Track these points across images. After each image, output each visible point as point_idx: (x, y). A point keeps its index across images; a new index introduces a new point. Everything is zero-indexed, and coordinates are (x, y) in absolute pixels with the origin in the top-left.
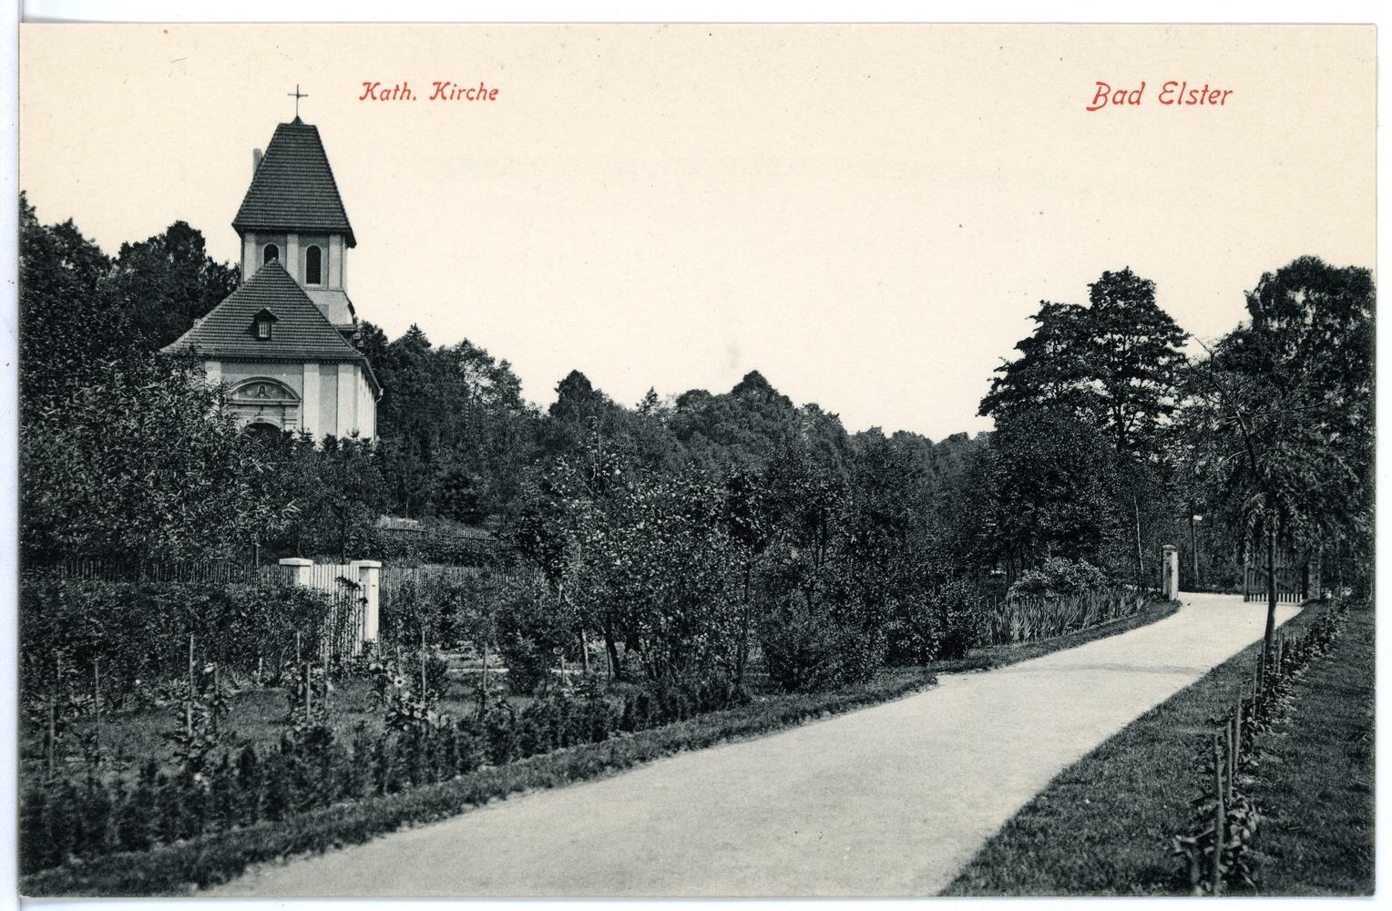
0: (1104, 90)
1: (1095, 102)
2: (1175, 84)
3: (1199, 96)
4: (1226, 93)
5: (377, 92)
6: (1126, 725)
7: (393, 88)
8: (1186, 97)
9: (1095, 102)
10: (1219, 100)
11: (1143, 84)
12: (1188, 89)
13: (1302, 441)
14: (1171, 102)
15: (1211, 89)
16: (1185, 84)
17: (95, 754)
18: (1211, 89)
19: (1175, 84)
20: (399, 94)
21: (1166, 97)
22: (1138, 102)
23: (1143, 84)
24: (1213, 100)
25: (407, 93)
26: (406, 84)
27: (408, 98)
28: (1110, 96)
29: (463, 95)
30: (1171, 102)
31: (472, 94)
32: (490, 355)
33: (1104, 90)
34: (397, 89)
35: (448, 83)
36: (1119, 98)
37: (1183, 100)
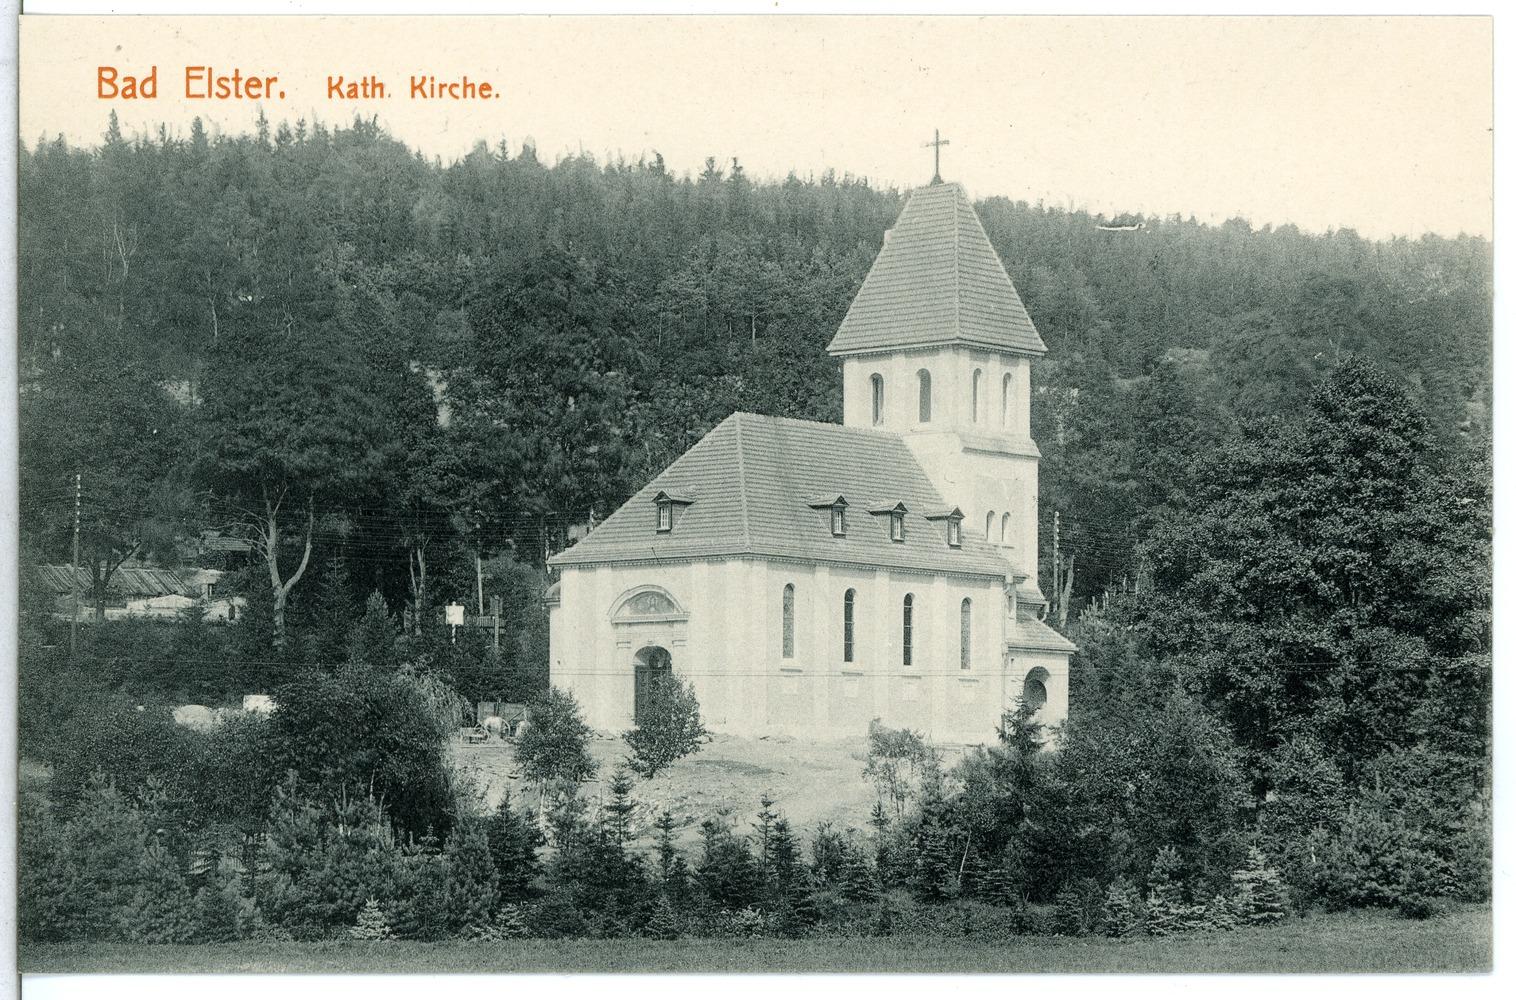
7: (359, 82)
13: (574, 928)
14: (259, 95)
15: (245, 76)
17: (1331, 459)
18: (245, 76)
22: (154, 94)
23: (154, 68)
24: (129, 83)
25: (378, 90)
27: (382, 95)
29: (446, 91)
30: (259, 95)
31: (456, 91)
32: (1134, 213)
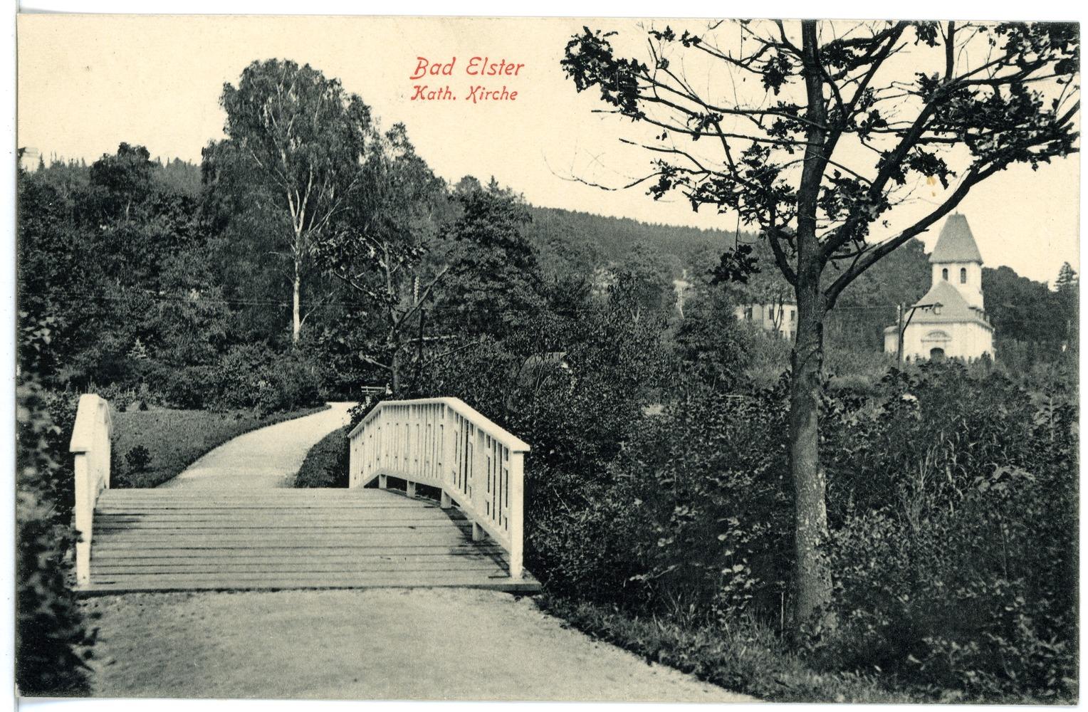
0: (424, 63)
1: (416, 73)
2: (480, 59)
3: (498, 69)
4: (519, 66)
5: (425, 93)
6: (302, 464)
7: (437, 90)
9: (416, 73)
10: (513, 71)
11: (454, 59)
12: (490, 63)
14: (476, 73)
15: (507, 63)
16: (487, 59)
18: (507, 63)
19: (480, 59)
20: (442, 95)
21: (472, 69)
22: (450, 73)
23: (454, 59)
28: (428, 69)
29: (490, 96)
30: (476, 73)
31: (496, 95)
33: (424, 63)
34: (441, 91)
35: (479, 87)
36: (435, 70)
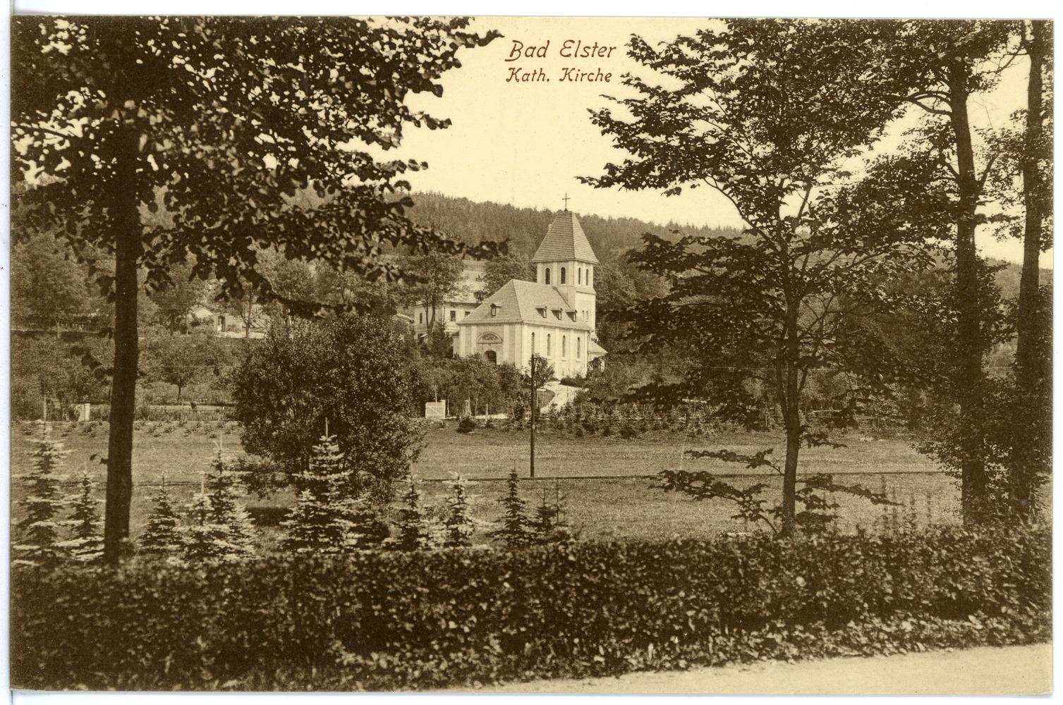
0: (519, 46)
1: (511, 55)
2: (573, 42)
3: (590, 52)
8: (581, 52)
9: (511, 55)
10: (606, 54)
14: (569, 55)
15: (600, 46)
19: (573, 42)
20: (537, 76)
21: (566, 52)
22: (544, 56)
26: (622, 76)
28: (523, 51)
29: (585, 78)
30: (569, 55)
33: (519, 46)
34: (535, 73)
36: (530, 52)
37: (578, 54)
